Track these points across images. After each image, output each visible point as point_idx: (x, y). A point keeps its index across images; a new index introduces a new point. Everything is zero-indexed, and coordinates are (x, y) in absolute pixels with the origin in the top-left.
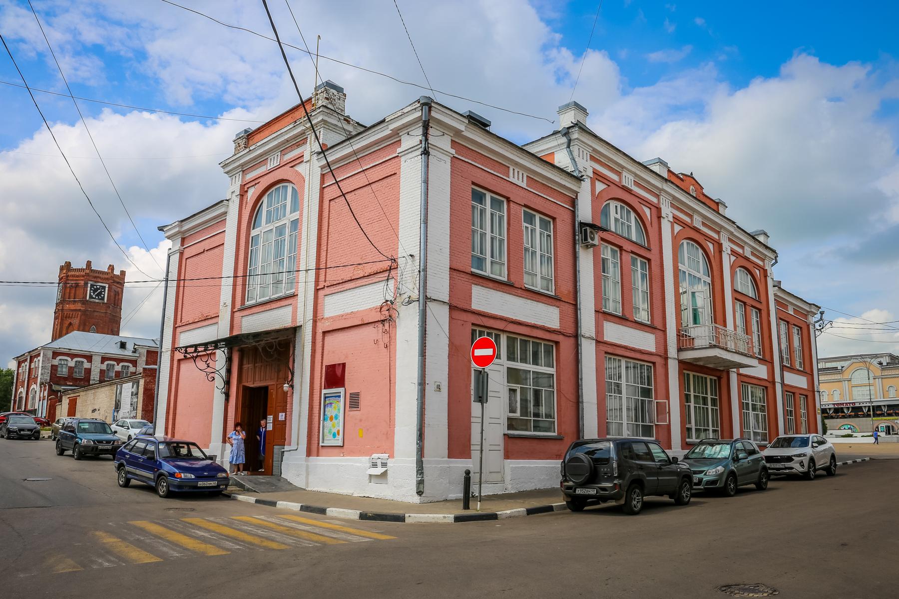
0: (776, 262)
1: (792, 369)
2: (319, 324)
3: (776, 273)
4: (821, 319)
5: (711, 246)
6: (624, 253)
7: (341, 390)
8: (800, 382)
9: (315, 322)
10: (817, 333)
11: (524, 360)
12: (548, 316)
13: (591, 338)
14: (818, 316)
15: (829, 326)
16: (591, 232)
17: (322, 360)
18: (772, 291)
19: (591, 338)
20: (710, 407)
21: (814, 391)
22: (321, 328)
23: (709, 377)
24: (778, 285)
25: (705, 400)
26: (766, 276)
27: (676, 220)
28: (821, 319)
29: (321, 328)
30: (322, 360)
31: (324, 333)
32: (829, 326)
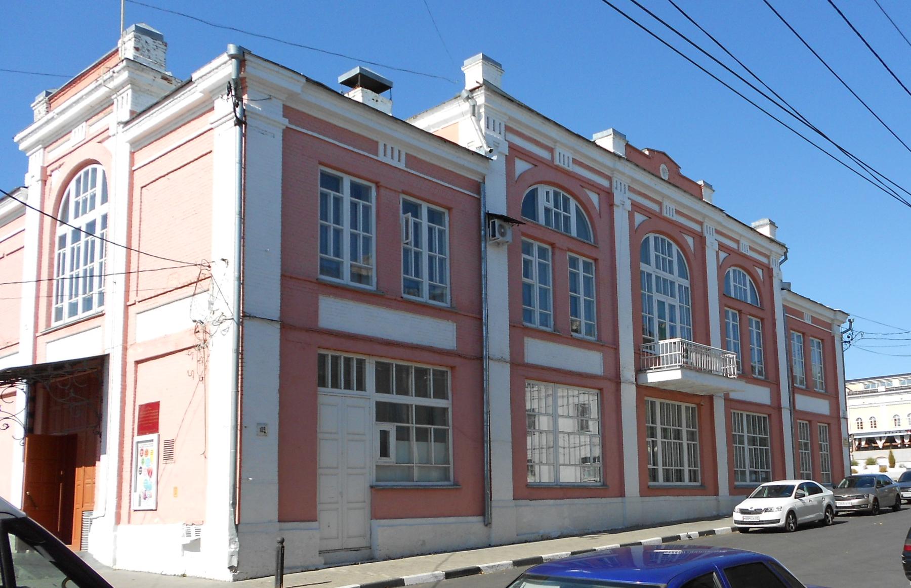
0: (786, 258)
1: (809, 391)
2: (130, 352)
3: (786, 273)
4: (850, 329)
5: (760, 271)
6: (557, 251)
7: (154, 436)
8: (821, 406)
9: (125, 349)
10: (845, 346)
11: (403, 390)
12: (440, 333)
13: (501, 360)
14: (846, 326)
15: (859, 337)
16: (501, 226)
17: (135, 398)
18: (779, 298)
19: (501, 360)
20: (685, 443)
21: (839, 418)
22: (132, 357)
23: (683, 406)
24: (786, 287)
25: (678, 434)
26: (771, 277)
27: (722, 247)
28: (850, 329)
29: (132, 357)
30: (135, 398)
31: (138, 362)
32: (859, 337)
